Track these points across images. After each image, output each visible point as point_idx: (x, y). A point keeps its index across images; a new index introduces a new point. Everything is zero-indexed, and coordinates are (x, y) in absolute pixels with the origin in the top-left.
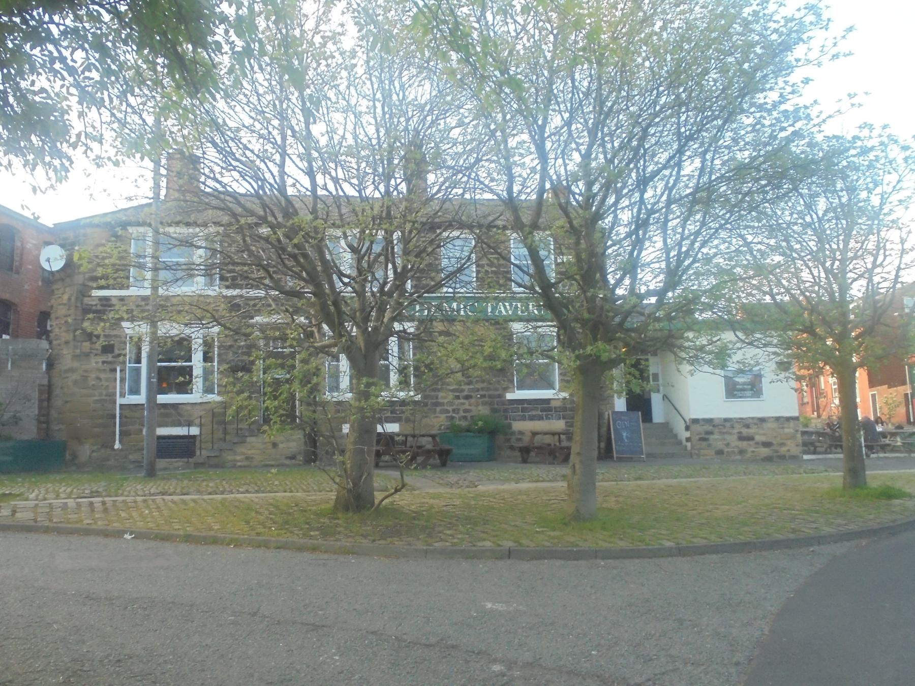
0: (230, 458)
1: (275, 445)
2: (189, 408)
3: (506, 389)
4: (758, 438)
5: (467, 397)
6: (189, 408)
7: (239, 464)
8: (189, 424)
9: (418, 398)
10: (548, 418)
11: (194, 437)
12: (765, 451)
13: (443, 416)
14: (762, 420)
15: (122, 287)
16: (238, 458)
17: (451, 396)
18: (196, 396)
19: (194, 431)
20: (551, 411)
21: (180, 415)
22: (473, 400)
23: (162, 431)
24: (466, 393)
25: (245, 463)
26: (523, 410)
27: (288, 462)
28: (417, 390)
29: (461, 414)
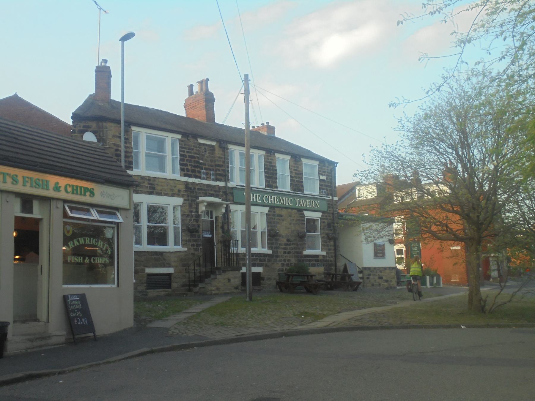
0: (210, 288)
1: (229, 280)
2: (168, 255)
3: (303, 249)
4: (384, 278)
5: (289, 253)
6: (168, 255)
7: (214, 292)
8: (169, 265)
9: (270, 252)
10: (318, 266)
11: (169, 275)
12: (386, 284)
13: (280, 263)
14: (385, 268)
15: (162, 152)
16: (213, 288)
17: (282, 251)
18: (171, 247)
19: (171, 270)
20: (318, 261)
21: (165, 260)
22: (291, 254)
23: (148, 270)
24: (288, 250)
25: (216, 292)
26: (310, 261)
27: (235, 291)
28: (269, 248)
29: (287, 262)
